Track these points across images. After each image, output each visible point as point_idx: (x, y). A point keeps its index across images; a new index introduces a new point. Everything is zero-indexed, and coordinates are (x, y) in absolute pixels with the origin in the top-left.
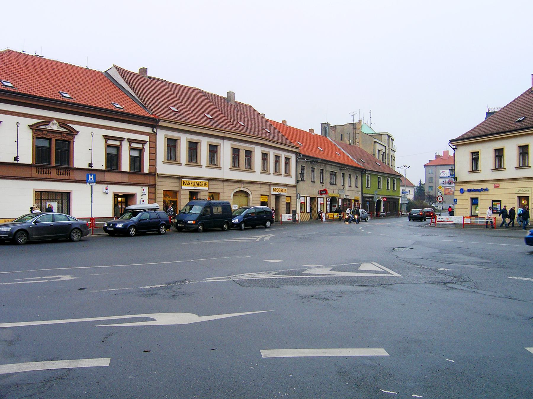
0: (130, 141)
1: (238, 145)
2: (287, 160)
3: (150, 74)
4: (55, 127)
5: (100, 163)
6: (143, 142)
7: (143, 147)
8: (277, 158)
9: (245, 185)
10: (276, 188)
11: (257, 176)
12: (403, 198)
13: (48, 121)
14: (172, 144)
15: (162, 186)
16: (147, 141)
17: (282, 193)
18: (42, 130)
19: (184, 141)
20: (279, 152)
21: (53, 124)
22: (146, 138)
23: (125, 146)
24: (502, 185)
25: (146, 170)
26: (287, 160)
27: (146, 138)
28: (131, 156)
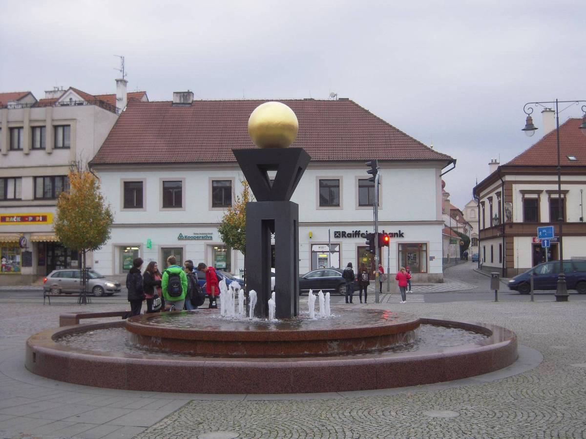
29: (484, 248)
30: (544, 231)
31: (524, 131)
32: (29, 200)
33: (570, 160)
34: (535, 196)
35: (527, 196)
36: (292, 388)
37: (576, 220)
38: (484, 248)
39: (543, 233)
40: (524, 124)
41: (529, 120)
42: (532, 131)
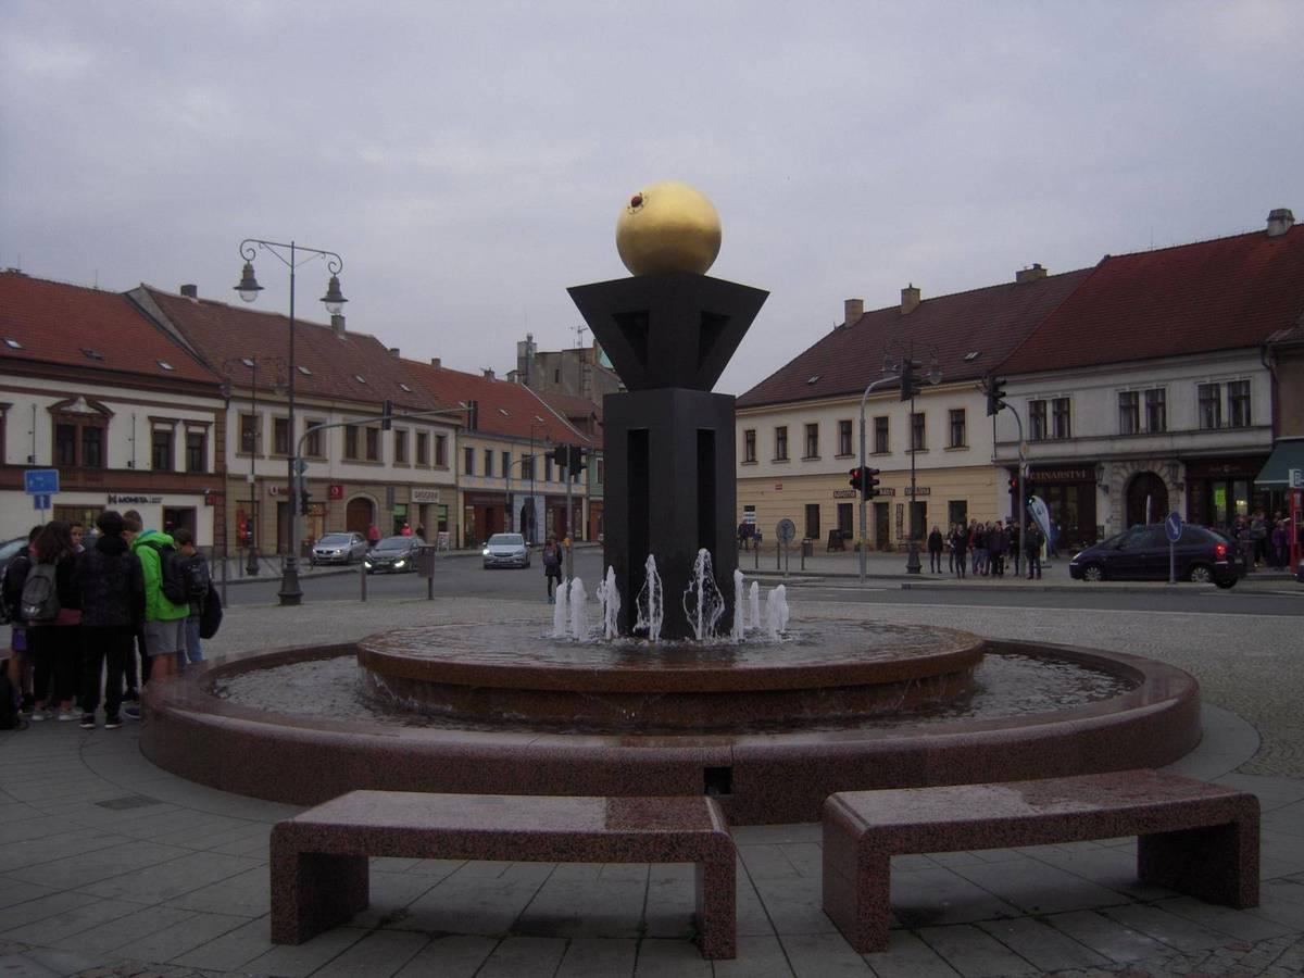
0: (187, 423)
1: (355, 419)
2: (441, 439)
3: (202, 294)
4: (82, 408)
5: (144, 462)
6: (206, 424)
7: (206, 433)
8: (422, 438)
9: (367, 488)
10: (421, 490)
11: (387, 472)
12: (222, 538)
13: (72, 398)
14: (249, 424)
15: (236, 493)
16: (211, 423)
17: (430, 501)
18: (65, 414)
19: (267, 417)
20: (424, 428)
21: (80, 403)
22: (210, 417)
23: (180, 432)
24: (786, 485)
25: (211, 469)
26: (441, 439)
27: (210, 417)
28: (257, 476)
29: (952, 571)
30: (40, 479)
31: (237, 291)
32: (1111, 438)
33: (9, 346)
34: (167, 427)
35: (159, 427)
36: (1103, 820)
37: (123, 465)
38: (952, 571)
39: (37, 483)
40: (238, 277)
41: (248, 271)
42: (254, 292)
